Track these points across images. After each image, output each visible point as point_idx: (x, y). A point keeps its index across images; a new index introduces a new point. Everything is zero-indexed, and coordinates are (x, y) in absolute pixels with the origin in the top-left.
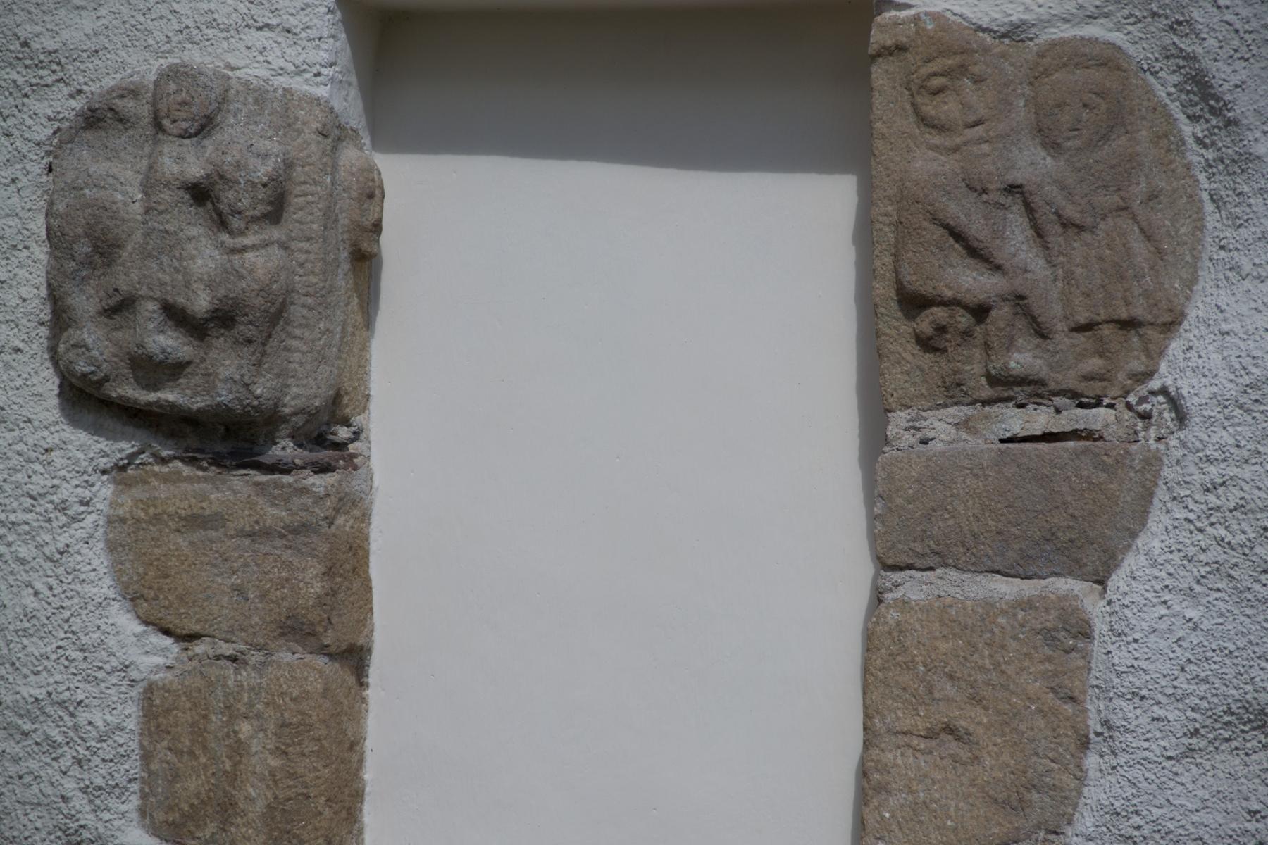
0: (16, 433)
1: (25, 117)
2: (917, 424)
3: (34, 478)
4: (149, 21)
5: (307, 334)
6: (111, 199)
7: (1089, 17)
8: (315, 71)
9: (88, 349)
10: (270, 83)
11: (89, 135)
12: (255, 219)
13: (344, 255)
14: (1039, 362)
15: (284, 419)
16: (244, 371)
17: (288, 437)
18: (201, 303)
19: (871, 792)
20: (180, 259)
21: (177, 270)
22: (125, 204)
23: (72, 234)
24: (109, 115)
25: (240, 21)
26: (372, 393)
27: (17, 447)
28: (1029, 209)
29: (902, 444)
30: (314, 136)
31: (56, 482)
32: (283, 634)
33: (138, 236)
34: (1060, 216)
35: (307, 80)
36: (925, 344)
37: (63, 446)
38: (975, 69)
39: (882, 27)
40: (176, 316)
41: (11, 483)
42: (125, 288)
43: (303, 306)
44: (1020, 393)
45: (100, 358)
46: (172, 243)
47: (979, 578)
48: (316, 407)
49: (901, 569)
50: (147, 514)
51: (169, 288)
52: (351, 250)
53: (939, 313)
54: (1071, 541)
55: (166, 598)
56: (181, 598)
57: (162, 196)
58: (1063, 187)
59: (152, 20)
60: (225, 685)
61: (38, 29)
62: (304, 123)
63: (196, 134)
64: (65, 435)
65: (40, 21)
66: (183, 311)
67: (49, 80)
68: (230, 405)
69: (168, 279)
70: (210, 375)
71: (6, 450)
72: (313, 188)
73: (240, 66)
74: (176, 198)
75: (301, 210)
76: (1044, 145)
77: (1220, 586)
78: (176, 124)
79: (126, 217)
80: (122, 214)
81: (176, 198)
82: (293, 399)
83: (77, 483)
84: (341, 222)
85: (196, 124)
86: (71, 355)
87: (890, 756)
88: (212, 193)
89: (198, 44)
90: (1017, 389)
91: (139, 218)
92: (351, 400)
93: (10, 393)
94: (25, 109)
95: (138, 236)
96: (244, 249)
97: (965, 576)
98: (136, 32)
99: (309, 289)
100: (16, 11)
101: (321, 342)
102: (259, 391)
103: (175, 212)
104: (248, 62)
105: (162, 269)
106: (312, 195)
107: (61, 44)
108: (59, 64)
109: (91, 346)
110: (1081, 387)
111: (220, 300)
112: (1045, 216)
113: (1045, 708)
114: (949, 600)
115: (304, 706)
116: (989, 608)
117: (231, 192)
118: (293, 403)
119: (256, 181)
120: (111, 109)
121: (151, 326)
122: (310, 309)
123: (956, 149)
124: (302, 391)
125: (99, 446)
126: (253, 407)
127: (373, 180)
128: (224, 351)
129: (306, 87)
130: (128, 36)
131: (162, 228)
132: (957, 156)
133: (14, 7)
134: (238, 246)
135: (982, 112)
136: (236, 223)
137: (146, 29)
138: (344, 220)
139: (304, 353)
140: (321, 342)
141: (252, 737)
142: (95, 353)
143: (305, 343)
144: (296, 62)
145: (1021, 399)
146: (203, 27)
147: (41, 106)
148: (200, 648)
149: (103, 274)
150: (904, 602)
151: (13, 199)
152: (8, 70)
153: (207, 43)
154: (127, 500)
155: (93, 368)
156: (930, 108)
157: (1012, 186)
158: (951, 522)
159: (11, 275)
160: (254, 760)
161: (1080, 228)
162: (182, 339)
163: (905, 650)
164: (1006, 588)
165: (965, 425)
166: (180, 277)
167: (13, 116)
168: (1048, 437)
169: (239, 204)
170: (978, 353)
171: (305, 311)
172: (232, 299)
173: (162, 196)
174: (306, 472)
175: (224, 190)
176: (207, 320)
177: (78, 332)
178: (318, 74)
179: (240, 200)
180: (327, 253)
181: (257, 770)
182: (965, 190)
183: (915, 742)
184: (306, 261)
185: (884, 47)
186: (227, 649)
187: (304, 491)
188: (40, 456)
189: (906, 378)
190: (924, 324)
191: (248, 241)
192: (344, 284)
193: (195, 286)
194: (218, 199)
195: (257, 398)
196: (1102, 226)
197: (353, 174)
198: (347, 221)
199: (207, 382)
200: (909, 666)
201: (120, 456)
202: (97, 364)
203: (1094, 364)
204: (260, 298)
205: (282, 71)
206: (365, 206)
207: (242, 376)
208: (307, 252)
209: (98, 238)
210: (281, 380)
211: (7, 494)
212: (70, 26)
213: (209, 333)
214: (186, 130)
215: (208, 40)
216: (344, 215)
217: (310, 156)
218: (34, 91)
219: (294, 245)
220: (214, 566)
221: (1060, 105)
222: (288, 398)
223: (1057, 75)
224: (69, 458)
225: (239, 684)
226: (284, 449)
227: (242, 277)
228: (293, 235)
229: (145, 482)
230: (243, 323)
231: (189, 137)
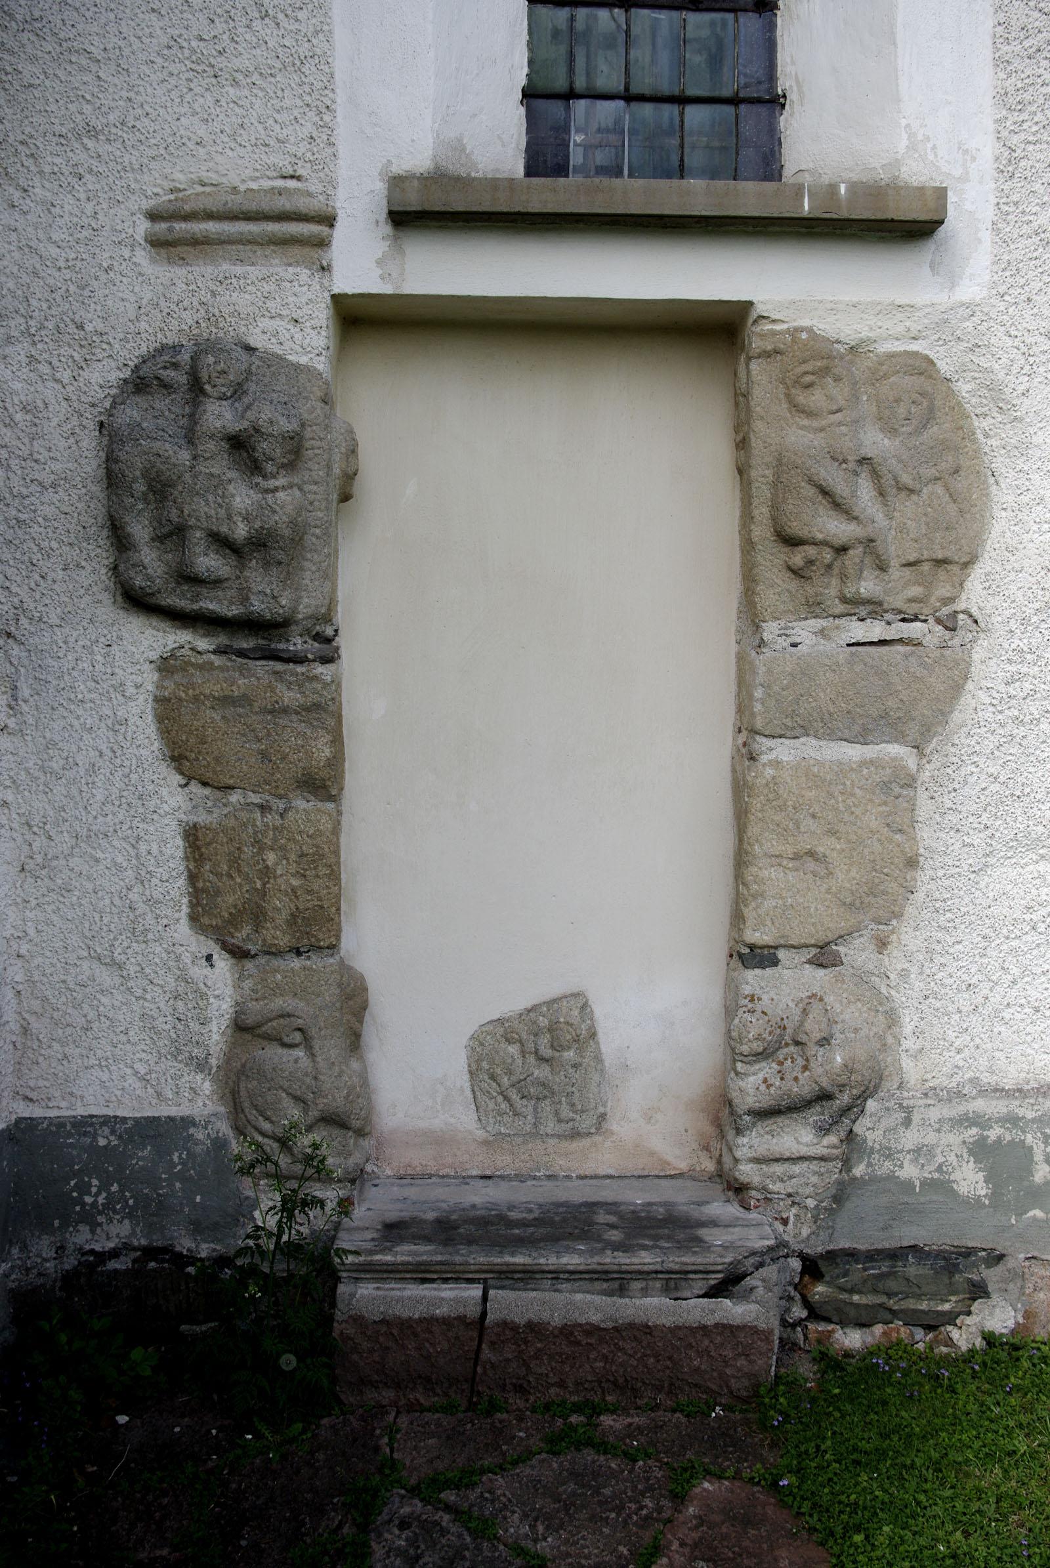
2: (787, 632)
7: (914, 338)
9: (145, 568)
12: (283, 466)
14: (878, 588)
18: (241, 531)
19: (750, 898)
28: (875, 475)
29: (778, 647)
32: (298, 787)
34: (897, 482)
36: (795, 572)
38: (836, 371)
39: (762, 336)
40: (222, 542)
43: (313, 535)
44: (863, 611)
47: (832, 744)
49: (774, 737)
50: (187, 694)
53: (811, 551)
54: (899, 718)
55: (204, 759)
56: (217, 759)
58: (900, 461)
60: (254, 825)
66: (226, 538)
69: (213, 513)
70: (243, 589)
72: (318, 443)
76: (882, 430)
77: (1011, 751)
79: (177, 462)
80: (173, 460)
87: (766, 872)
90: (862, 608)
96: (276, 489)
97: (822, 743)
102: (284, 602)
108: (109, 344)
110: (904, 607)
112: (887, 481)
113: (883, 838)
114: (812, 762)
115: (318, 841)
116: (842, 769)
123: (822, 430)
132: (822, 435)
135: (842, 403)
136: (269, 467)
138: (337, 471)
141: (277, 864)
145: (863, 614)
148: (235, 797)
150: (778, 763)
154: (169, 684)
156: (801, 398)
157: (864, 459)
158: (814, 704)
160: (279, 881)
161: (912, 491)
162: (221, 561)
163: (778, 797)
164: (853, 752)
165: (822, 633)
168: (883, 642)
170: (835, 582)
171: (314, 539)
176: (244, 545)
181: (283, 888)
182: (829, 459)
183: (785, 863)
185: (765, 352)
186: (255, 799)
187: (316, 678)
189: (777, 597)
190: (797, 559)
193: (235, 518)
194: (254, 449)
196: (925, 490)
200: (782, 808)
203: (915, 591)
208: (315, 493)
213: (309, 556)
214: (224, 394)
220: (244, 735)
221: (898, 400)
223: (892, 379)
225: (266, 825)
227: (275, 512)
229: (184, 670)
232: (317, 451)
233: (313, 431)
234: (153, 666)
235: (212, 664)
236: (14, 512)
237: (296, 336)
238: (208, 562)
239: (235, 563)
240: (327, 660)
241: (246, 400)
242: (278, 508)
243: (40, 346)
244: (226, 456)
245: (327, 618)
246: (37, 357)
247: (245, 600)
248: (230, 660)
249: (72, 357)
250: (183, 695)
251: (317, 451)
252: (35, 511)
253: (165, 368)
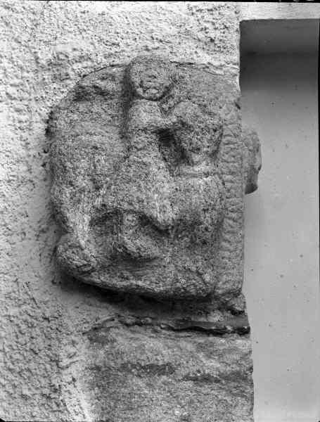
15: (217, 298)
43: (229, 218)
82: (224, 283)
86: (69, 253)
109: (84, 246)
142: (86, 251)
171: (231, 222)
174: (235, 335)
195: (205, 283)
208: (232, 182)
222: (221, 283)
226: (216, 318)
231: (155, 100)
232: (232, 146)
238: (137, 242)
240: (244, 332)
241: (171, 102)
245: (236, 293)
250: (112, 364)
253: (103, 79)
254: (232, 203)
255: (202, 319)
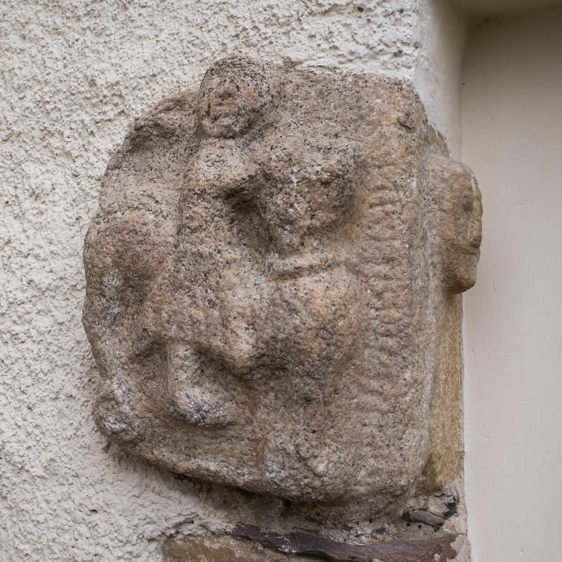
0: (65, 489)
1: (90, 155)
3: (80, 541)
4: (205, 33)
5: (387, 387)
6: (142, 220)
8: (396, 50)
9: (117, 403)
10: (338, 71)
11: (136, 159)
12: (311, 231)
13: (434, 283)
15: (358, 500)
16: (299, 441)
17: (365, 520)
20: (217, 289)
21: (212, 304)
22: (157, 225)
23: (101, 266)
24: (155, 133)
25: (302, 10)
26: (466, 449)
27: (65, 505)
30: (394, 129)
31: (100, 550)
33: (170, 264)
35: (384, 63)
37: (106, 508)
41: (59, 543)
42: (153, 328)
43: (382, 349)
45: (131, 414)
46: (206, 269)
48: (402, 487)
51: (203, 328)
52: (442, 276)
57: (196, 209)
59: (209, 31)
61: (104, 66)
62: (382, 113)
63: (242, 133)
64: (109, 496)
65: (106, 58)
67: (111, 115)
68: (283, 485)
69: (200, 315)
70: (258, 441)
71: (56, 507)
73: (301, 58)
74: (212, 211)
75: (378, 223)
78: (217, 122)
80: (153, 237)
81: (212, 211)
83: (120, 554)
84: (431, 240)
85: (241, 120)
88: (257, 202)
89: (255, 46)
91: (171, 240)
92: (444, 465)
93: (62, 444)
94: (91, 148)
95: (170, 264)
96: (297, 273)
98: (192, 48)
99: (390, 327)
100: (87, 54)
101: (408, 399)
102: (321, 468)
103: (211, 229)
104: (311, 52)
105: (194, 303)
106: (393, 203)
107: (122, 75)
108: (120, 96)
109: (120, 400)
111: (267, 343)
117: (280, 196)
118: (369, 480)
119: (314, 178)
120: (157, 125)
121: (183, 376)
122: (391, 353)
124: (382, 465)
125: (144, 511)
126: (313, 488)
127: (470, 189)
128: (276, 410)
129: (381, 72)
130: (185, 53)
131: (194, 250)
133: (86, 50)
134: (290, 268)
137: (202, 42)
139: (383, 413)
140: (408, 399)
142: (126, 408)
143: (385, 400)
144: (371, 42)
146: (261, 26)
147: (104, 142)
149: (136, 312)
151: (76, 239)
152: (79, 112)
153: (266, 42)
155: (124, 426)
159: (69, 317)
166: (216, 313)
167: (81, 156)
169: (291, 210)
172: (283, 340)
173: (196, 209)
175: (271, 195)
177: (108, 382)
178: (399, 54)
179: (292, 206)
180: (413, 279)
184: (385, 290)
188: (86, 517)
191: (303, 261)
192: (435, 321)
194: (265, 209)
195: (319, 476)
197: (444, 180)
198: (438, 240)
199: (255, 450)
201: (166, 525)
202: (127, 421)
204: (319, 340)
205: (354, 56)
206: (462, 220)
207: (297, 446)
208: (386, 277)
209: (129, 268)
210: (353, 451)
211: (56, 556)
212: (132, 57)
214: (228, 127)
215: (266, 38)
216: (434, 231)
217: (388, 154)
218: (99, 128)
219: (368, 269)
222: (363, 473)
224: (112, 524)
227: (294, 311)
228: (367, 255)
230: (298, 375)
231: (233, 137)
233: (384, 175)
234: (153, 546)
235: (231, 553)
236: (8, 323)
237: (360, 32)
239: (242, 398)
242: (298, 304)
243: (53, 115)
244: (224, 224)
246: (50, 128)
247: (259, 460)
248: (257, 551)
249: (82, 121)
251: (389, 207)
252: (30, 322)
254: (386, 320)
255: (338, 536)
